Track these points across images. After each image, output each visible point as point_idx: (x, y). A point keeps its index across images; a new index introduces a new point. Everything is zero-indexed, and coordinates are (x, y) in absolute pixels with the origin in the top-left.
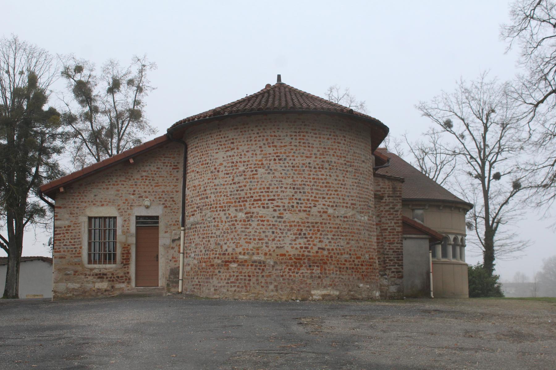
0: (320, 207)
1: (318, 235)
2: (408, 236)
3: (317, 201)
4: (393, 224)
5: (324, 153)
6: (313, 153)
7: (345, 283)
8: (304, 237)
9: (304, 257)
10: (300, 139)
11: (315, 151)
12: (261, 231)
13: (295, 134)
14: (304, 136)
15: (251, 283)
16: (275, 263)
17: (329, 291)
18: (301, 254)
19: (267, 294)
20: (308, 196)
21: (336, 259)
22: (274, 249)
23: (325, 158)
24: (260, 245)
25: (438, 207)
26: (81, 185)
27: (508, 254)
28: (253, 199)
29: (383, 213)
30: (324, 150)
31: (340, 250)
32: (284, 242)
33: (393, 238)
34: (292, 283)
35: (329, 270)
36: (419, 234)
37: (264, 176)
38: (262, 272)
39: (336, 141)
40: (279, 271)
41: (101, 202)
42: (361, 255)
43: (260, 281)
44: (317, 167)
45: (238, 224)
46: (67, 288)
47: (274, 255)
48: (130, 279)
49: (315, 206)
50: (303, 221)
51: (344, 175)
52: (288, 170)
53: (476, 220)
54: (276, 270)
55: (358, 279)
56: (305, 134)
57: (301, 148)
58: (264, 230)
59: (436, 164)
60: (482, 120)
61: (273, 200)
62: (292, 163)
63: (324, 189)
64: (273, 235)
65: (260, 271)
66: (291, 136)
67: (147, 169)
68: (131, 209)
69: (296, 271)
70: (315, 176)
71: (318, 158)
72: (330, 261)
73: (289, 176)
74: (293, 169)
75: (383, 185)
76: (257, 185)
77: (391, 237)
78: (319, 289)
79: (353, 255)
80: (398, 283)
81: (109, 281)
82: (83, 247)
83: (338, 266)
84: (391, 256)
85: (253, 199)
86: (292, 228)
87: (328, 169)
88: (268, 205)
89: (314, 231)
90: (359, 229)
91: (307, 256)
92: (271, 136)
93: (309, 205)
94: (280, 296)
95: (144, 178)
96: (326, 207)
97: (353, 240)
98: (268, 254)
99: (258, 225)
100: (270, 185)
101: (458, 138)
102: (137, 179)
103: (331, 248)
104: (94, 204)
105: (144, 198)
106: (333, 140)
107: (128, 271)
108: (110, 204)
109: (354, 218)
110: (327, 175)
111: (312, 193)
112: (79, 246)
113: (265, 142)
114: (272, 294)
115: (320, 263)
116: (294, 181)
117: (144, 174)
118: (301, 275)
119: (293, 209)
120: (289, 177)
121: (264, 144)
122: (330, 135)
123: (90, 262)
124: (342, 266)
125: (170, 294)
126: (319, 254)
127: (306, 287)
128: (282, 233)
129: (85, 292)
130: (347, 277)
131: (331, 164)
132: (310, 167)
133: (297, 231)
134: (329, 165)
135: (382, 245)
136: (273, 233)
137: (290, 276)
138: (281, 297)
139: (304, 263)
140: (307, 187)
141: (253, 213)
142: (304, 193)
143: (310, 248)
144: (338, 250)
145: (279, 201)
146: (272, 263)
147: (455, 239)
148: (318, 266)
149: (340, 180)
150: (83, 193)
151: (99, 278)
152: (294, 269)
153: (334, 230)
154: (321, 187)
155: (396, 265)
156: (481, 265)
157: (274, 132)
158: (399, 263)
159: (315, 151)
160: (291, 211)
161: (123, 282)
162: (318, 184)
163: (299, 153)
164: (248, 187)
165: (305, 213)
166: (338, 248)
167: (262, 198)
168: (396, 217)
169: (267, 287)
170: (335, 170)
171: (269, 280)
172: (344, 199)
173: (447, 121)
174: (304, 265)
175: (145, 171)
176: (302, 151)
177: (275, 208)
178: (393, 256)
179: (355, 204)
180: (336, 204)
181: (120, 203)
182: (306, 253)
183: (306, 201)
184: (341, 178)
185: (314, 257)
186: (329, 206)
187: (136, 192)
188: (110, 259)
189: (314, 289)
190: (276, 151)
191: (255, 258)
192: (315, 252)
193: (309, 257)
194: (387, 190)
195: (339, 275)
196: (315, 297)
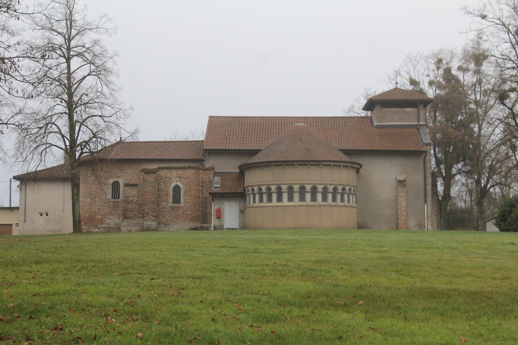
77: (148, 205)
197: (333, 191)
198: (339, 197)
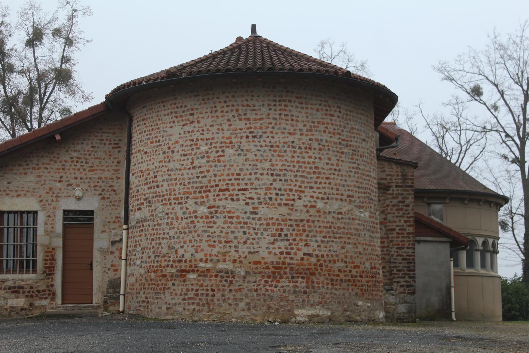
0: (306, 199)
1: (304, 237)
2: (423, 238)
3: (303, 192)
4: (402, 223)
5: (313, 129)
8: (285, 238)
10: (280, 110)
11: (300, 125)
12: (229, 230)
13: (274, 103)
14: (286, 106)
15: (215, 299)
16: (247, 273)
17: (317, 311)
18: (281, 261)
19: (236, 314)
20: (290, 185)
21: (327, 269)
22: (245, 255)
24: (228, 249)
25: (462, 200)
28: (218, 189)
29: (389, 208)
30: (312, 125)
31: (332, 256)
32: (259, 246)
33: (403, 241)
34: (269, 300)
35: (318, 283)
37: (233, 158)
39: (328, 113)
40: (252, 284)
41: (17, 191)
42: (361, 263)
43: (227, 297)
44: (303, 146)
47: (245, 262)
48: (54, 294)
49: (300, 199)
50: (284, 218)
51: (338, 158)
52: (265, 151)
53: (512, 219)
54: (248, 282)
55: (356, 294)
56: (287, 103)
57: (281, 121)
58: (233, 229)
59: (460, 144)
61: (245, 190)
62: (270, 142)
63: (312, 175)
64: (245, 237)
65: (227, 284)
66: (269, 105)
67: (78, 148)
69: (275, 283)
70: (299, 159)
71: (304, 135)
72: (319, 271)
73: (265, 158)
74: (272, 149)
76: (224, 170)
77: (400, 239)
78: (304, 308)
79: (349, 263)
80: (409, 301)
81: (27, 296)
83: (329, 278)
84: (399, 265)
85: (218, 189)
86: (269, 227)
87: (318, 149)
90: (357, 230)
91: (289, 264)
92: (243, 106)
93: (292, 197)
94: (253, 317)
95: (75, 159)
97: (349, 243)
98: (238, 262)
99: (225, 223)
100: (241, 170)
101: (489, 110)
102: (66, 161)
103: (320, 254)
106: (324, 112)
107: (52, 283)
110: (316, 158)
113: (234, 113)
114: (243, 314)
115: (306, 274)
116: (272, 165)
117: (74, 154)
119: (271, 202)
120: (266, 160)
121: (234, 116)
126: (305, 262)
127: (288, 305)
128: (256, 234)
130: (342, 291)
131: (321, 143)
133: (276, 231)
134: (319, 144)
135: (387, 250)
136: (245, 233)
137: (267, 290)
139: (285, 273)
140: (289, 173)
141: (218, 207)
142: (286, 180)
143: (292, 253)
144: (330, 256)
145: (253, 191)
146: (243, 273)
147: (485, 243)
148: (303, 278)
149: (333, 165)
151: (13, 292)
152: (272, 281)
153: (325, 230)
154: (309, 173)
155: (407, 277)
156: (520, 278)
157: (247, 100)
158: (410, 274)
159: (300, 125)
160: (268, 204)
161: (46, 298)
162: (303, 169)
163: (279, 129)
165: (287, 207)
166: (330, 253)
167: (231, 188)
169: (237, 305)
170: (327, 151)
171: (238, 295)
172: (337, 189)
173: (475, 87)
174: (285, 277)
175: (75, 151)
176: (283, 125)
177: (248, 201)
178: (402, 265)
179: (352, 196)
180: (328, 195)
182: (288, 261)
183: (288, 192)
184: (334, 161)
186: (318, 198)
187: (64, 179)
189: (298, 307)
190: (248, 126)
191: (221, 266)
194: (395, 177)
195: (331, 289)
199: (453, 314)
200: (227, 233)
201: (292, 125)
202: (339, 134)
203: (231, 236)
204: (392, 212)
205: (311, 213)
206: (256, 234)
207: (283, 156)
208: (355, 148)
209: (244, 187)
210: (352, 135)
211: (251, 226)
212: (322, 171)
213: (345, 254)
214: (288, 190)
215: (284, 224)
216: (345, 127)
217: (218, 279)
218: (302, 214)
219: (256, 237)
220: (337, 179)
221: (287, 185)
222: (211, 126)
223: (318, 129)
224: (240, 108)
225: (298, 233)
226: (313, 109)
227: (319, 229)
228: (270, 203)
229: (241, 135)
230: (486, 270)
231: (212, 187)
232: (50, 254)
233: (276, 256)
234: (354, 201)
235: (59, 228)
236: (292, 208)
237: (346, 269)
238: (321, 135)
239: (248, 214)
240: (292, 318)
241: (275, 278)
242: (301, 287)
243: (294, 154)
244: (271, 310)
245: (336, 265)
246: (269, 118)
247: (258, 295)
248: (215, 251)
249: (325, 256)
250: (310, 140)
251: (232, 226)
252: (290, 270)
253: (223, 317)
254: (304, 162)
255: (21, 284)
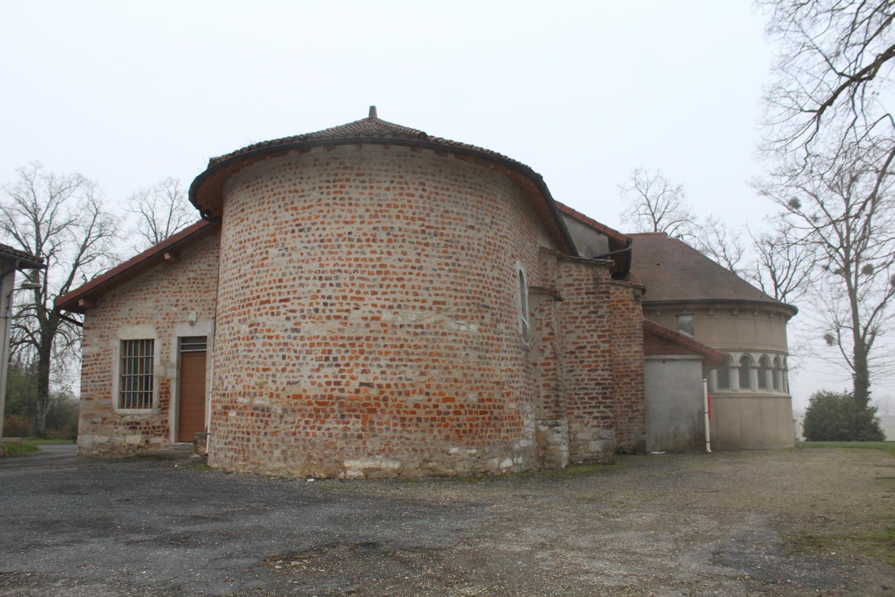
0: (366, 309)
1: (361, 360)
2: (668, 357)
3: (362, 299)
4: (595, 338)
5: (379, 214)
6: (357, 214)
7: (414, 446)
8: (334, 363)
9: (333, 401)
10: (335, 192)
11: (361, 210)
12: (267, 354)
13: (327, 184)
14: (342, 187)
15: (250, 444)
16: (285, 410)
17: (378, 462)
18: (327, 394)
19: (270, 465)
20: (344, 291)
21: (395, 404)
22: (283, 386)
23: (380, 222)
24: (264, 379)
25: (731, 311)
26: (114, 296)
27: (889, 378)
28: (259, 300)
29: (578, 321)
30: (378, 208)
31: (404, 386)
32: (300, 374)
33: (596, 361)
34: (310, 447)
35: (380, 424)
36: (690, 354)
37: (276, 260)
38: (265, 427)
39: (406, 191)
40: (290, 426)
41: (136, 318)
42: (457, 394)
43: (262, 442)
44: (363, 238)
45: (241, 344)
46: (94, 443)
47: (283, 396)
48: (168, 431)
49: (357, 309)
50: (334, 335)
51: (419, 251)
52: (313, 248)
53: (838, 331)
54: (286, 422)
55: (447, 438)
56: (344, 183)
57: (335, 207)
58: (271, 353)
59: (788, 260)
60: (842, 195)
61: (286, 300)
62: (320, 235)
63: (376, 276)
64: (284, 362)
65: (262, 425)
66: (320, 188)
67: (195, 267)
68: (173, 327)
69: (318, 424)
70: (358, 256)
71: (366, 223)
72: (383, 406)
73: (313, 257)
74: (322, 244)
75: (578, 275)
76: (266, 276)
77: (593, 359)
78: (358, 458)
79: (434, 394)
80: (605, 436)
81: (143, 433)
82: (114, 384)
83: (398, 416)
84: (592, 391)
85: (259, 300)
86: (313, 348)
87: (386, 240)
88: (279, 310)
89: (354, 352)
90: (451, 348)
91: (338, 398)
92: (290, 192)
93: (345, 307)
94: (290, 470)
95: (192, 280)
96: (379, 308)
97: (434, 368)
98: (275, 396)
99: (264, 345)
100: (284, 274)
101: (809, 222)
102: (183, 283)
103: (384, 383)
104: (128, 322)
105: (189, 310)
106: (398, 191)
107: (166, 418)
108: (147, 321)
109: (442, 327)
110: (382, 253)
111: (353, 285)
112: (108, 383)
113: (281, 203)
114: (278, 465)
115: (362, 411)
116: (322, 266)
117: (192, 275)
118: (326, 432)
119: (317, 315)
120: (314, 260)
121: (279, 207)
122: (392, 182)
123: (122, 406)
124: (408, 416)
125: (197, 456)
126: (361, 395)
127: (335, 455)
128: (298, 358)
129: (113, 448)
130: (420, 435)
131: (391, 233)
132: (350, 240)
133: (322, 353)
134: (388, 234)
135: (553, 374)
136: (284, 357)
137: (307, 434)
138: (292, 471)
139: (333, 411)
140: (343, 275)
141: (258, 324)
142: (338, 285)
143: (343, 383)
144: (400, 386)
145: (296, 301)
146: (280, 411)
147: (763, 360)
148: (357, 417)
149: (410, 261)
150: (117, 306)
151: (131, 428)
152: (315, 421)
153: (393, 350)
154: (370, 273)
155: (602, 406)
156: (851, 394)
157: (295, 185)
158: (606, 403)
159: (361, 210)
160: (314, 318)
161: (160, 435)
162: (364, 269)
163: (332, 218)
164: (255, 281)
165: (338, 321)
166: (400, 382)
167: (272, 298)
168: (600, 327)
169: (272, 453)
170: (400, 243)
171: (274, 440)
172: (416, 294)
173: (792, 200)
174: (332, 415)
175: (192, 271)
176: (338, 212)
177: (290, 314)
178: (595, 391)
179: (444, 303)
180: (399, 303)
181: (159, 318)
182: (336, 393)
183: (341, 300)
184: (412, 256)
185: (351, 399)
186: (383, 307)
187: (180, 303)
188: (146, 401)
189: (351, 458)
190: (295, 217)
191: (258, 402)
192: (354, 391)
193: (342, 400)
194: (585, 282)
195: (401, 432)
196: (350, 473)
197: (740, 365)
198: (754, 375)
199: (708, 446)
200: (265, 358)
201: (350, 211)
202: (423, 220)
203: (269, 361)
204: (581, 325)
205: (372, 328)
206: (298, 358)
207: (336, 253)
208: (451, 238)
209: (285, 296)
210: (446, 221)
211: (292, 348)
212: (392, 270)
213: (427, 383)
214: (341, 298)
215: (333, 344)
216: (432, 210)
217: (254, 418)
218: (360, 330)
219: (298, 362)
220: (417, 280)
221: (340, 291)
222: (258, 222)
223: (387, 214)
224: (287, 195)
225: (353, 355)
226: (381, 188)
227: (383, 350)
228: (316, 317)
229: (286, 229)
230: (767, 390)
231: (253, 299)
232: (165, 385)
233: (320, 388)
234: (447, 310)
235: (174, 357)
236: (345, 321)
237: (427, 403)
238: (392, 222)
239: (289, 333)
240: (340, 473)
241: (318, 417)
242: (354, 430)
243: (350, 250)
244: (312, 461)
245: (410, 398)
246: (320, 205)
247: (296, 440)
248: (253, 381)
249: (393, 387)
250: (375, 229)
251: (271, 348)
252: (339, 407)
253: (257, 468)
254: (365, 260)
255: (138, 419)
